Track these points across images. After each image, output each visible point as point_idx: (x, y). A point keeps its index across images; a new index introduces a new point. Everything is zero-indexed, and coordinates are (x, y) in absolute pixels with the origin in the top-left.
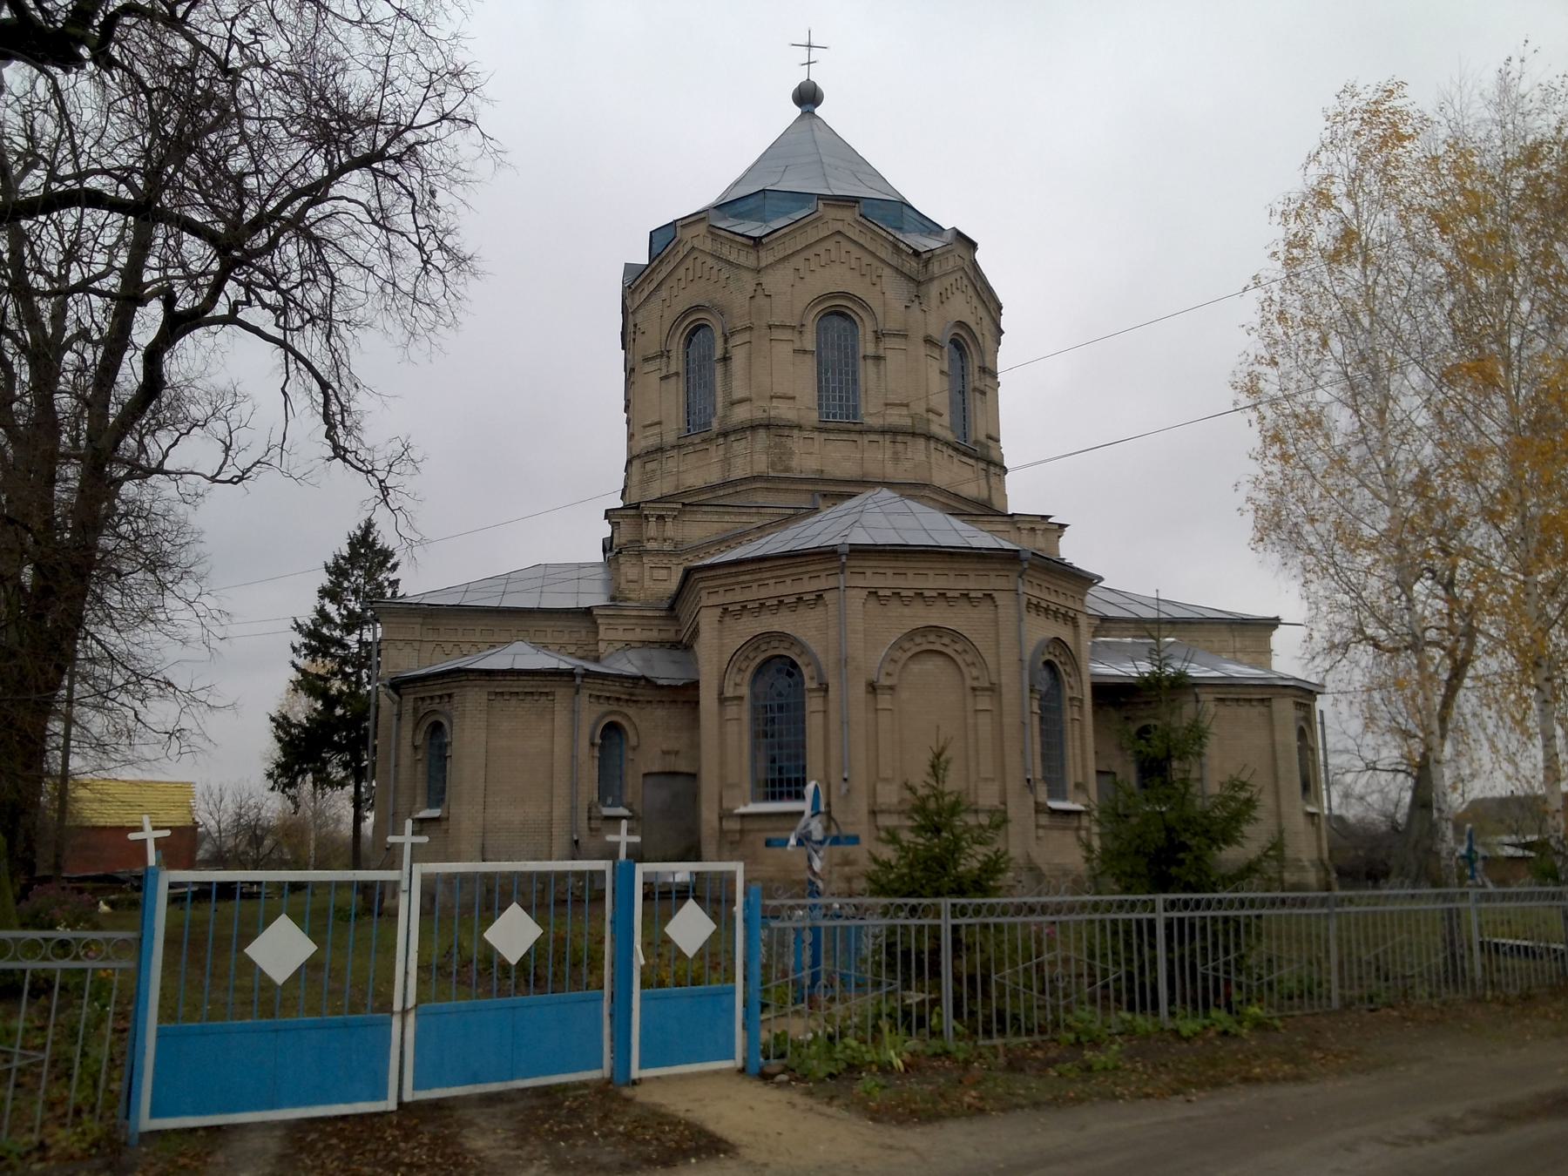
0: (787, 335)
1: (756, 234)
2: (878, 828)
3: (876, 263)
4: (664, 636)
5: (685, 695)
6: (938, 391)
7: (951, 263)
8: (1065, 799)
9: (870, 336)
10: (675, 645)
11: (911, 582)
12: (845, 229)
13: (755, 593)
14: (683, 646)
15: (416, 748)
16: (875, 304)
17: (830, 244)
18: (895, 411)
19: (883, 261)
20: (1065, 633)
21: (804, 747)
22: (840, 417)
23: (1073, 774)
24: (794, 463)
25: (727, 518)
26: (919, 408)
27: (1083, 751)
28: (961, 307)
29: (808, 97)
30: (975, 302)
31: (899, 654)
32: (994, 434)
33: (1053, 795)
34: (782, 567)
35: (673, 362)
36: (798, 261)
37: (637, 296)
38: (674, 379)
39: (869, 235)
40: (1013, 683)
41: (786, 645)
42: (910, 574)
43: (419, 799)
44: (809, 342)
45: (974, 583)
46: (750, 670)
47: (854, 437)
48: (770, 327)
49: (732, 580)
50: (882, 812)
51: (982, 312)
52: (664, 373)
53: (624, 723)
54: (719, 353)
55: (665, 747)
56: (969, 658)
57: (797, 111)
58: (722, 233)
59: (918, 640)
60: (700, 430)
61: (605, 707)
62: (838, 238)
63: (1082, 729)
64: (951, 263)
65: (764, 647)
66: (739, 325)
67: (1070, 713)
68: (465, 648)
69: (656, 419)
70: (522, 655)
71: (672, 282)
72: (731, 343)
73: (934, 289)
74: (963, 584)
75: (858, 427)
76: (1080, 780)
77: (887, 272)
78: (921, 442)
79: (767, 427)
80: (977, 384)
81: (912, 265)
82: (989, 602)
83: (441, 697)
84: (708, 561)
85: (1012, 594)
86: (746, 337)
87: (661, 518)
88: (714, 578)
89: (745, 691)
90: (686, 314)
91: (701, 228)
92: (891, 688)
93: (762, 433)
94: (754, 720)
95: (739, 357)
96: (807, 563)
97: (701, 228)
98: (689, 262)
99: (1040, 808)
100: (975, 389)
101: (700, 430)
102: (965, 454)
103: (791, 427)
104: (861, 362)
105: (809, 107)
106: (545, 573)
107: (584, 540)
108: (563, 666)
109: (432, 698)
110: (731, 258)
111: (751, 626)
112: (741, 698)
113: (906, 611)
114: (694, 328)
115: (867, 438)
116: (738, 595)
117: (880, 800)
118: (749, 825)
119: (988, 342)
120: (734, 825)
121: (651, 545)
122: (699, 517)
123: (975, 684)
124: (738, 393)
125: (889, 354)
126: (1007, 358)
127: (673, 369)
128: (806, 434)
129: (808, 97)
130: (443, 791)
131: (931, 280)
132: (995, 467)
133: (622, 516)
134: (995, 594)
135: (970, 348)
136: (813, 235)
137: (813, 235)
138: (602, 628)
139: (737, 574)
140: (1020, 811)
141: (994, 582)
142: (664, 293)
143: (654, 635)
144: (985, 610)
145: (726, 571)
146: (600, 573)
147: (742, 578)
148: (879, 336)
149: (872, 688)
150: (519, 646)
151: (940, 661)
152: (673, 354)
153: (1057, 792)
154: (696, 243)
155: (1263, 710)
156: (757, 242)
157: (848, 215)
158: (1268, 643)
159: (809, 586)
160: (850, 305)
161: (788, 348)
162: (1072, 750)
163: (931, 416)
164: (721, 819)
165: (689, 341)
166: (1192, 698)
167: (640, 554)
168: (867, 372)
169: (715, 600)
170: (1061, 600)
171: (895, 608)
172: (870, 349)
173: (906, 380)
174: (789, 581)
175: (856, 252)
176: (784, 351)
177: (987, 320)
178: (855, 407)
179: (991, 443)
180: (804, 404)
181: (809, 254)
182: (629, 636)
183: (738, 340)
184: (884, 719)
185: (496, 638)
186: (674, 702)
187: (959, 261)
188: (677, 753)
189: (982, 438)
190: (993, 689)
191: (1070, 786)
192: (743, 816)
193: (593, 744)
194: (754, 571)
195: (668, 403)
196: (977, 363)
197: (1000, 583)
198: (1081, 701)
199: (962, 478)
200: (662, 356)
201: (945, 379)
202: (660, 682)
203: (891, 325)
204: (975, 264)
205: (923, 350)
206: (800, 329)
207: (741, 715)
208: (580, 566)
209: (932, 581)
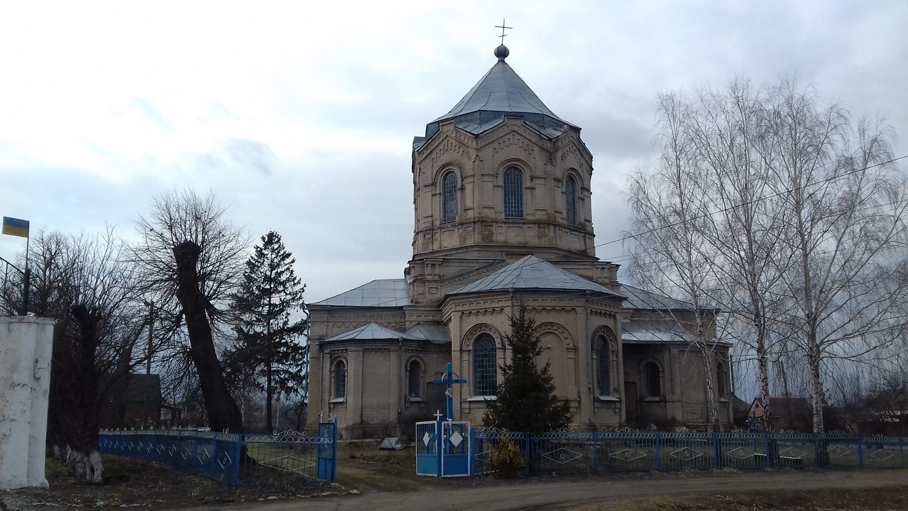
0: (490, 179)
3: (531, 144)
4: (435, 318)
5: (446, 348)
6: (561, 203)
7: (567, 140)
8: (609, 395)
9: (528, 178)
10: (438, 323)
14: (442, 324)
15: (331, 372)
17: (510, 136)
18: (539, 213)
20: (609, 322)
23: (613, 384)
24: (494, 238)
26: (550, 211)
27: (618, 375)
28: (572, 161)
29: (502, 53)
30: (579, 156)
32: (588, 218)
33: (602, 394)
34: (487, 296)
35: (438, 188)
36: (496, 145)
40: (584, 347)
42: (540, 300)
44: (500, 181)
45: (566, 303)
51: (583, 161)
54: (459, 186)
55: (437, 371)
56: (565, 335)
57: (497, 59)
60: (448, 220)
61: (409, 355)
63: (617, 365)
64: (567, 140)
66: (468, 174)
67: (612, 358)
70: (374, 331)
71: (437, 151)
72: (466, 181)
73: (559, 155)
74: (563, 304)
76: (616, 386)
77: (536, 149)
79: (482, 222)
80: (580, 195)
81: (548, 145)
84: (455, 292)
85: (583, 309)
86: (471, 179)
87: (433, 265)
89: (471, 348)
90: (444, 166)
91: (451, 127)
93: (478, 225)
94: (475, 361)
98: (445, 142)
99: (596, 400)
100: (579, 198)
101: (448, 220)
103: (493, 222)
104: (524, 191)
106: (377, 285)
107: (394, 267)
108: (395, 337)
112: (469, 351)
114: (446, 172)
115: (526, 226)
116: (467, 307)
118: (473, 406)
119: (585, 175)
120: (466, 406)
121: (429, 278)
124: (469, 204)
125: (537, 187)
126: (596, 183)
127: (438, 192)
129: (502, 53)
132: (589, 234)
135: (576, 183)
138: (407, 315)
140: (586, 400)
141: (575, 303)
142: (434, 155)
143: (430, 318)
144: (571, 316)
146: (402, 286)
148: (532, 178)
150: (373, 326)
151: (553, 337)
152: (438, 184)
153: (605, 391)
154: (449, 133)
156: (477, 137)
157: (519, 123)
161: (491, 185)
162: (613, 373)
163: (557, 214)
167: (424, 282)
168: (527, 196)
170: (608, 308)
173: (541, 199)
177: (585, 165)
178: (522, 211)
179: (587, 223)
181: (501, 141)
182: (420, 319)
186: (440, 351)
187: (571, 139)
189: (583, 221)
190: (575, 349)
191: (612, 389)
192: (470, 402)
195: (435, 208)
196: (580, 185)
197: (579, 304)
198: (617, 352)
199: (573, 242)
201: (564, 196)
203: (537, 174)
204: (579, 139)
205: (553, 183)
206: (496, 176)
208: (394, 281)
209: (549, 303)
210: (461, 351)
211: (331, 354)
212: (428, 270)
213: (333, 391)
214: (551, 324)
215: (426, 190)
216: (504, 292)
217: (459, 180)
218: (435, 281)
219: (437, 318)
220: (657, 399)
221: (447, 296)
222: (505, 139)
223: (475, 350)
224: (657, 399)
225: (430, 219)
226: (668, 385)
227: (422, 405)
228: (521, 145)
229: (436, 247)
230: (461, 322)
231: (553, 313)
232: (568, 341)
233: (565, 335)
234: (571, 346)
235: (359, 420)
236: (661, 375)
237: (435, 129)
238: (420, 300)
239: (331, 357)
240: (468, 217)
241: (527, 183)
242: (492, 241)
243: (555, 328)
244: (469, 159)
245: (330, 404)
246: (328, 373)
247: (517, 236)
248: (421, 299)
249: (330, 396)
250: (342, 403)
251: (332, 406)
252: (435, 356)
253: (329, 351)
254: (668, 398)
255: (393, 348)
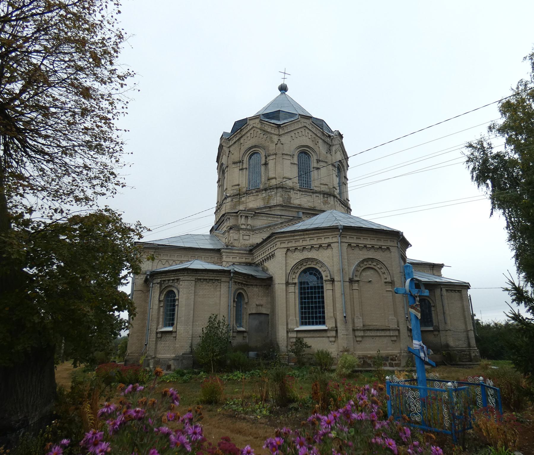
0: (289, 157)
1: (279, 123)
2: (356, 336)
3: (317, 138)
4: (247, 261)
9: (315, 161)
11: (362, 242)
12: (307, 126)
13: (300, 243)
15: (160, 301)
16: (317, 150)
17: (302, 130)
18: (322, 186)
19: (319, 137)
21: (323, 302)
22: (306, 188)
25: (269, 219)
29: (283, 89)
31: (359, 268)
34: (314, 234)
36: (292, 134)
37: (231, 142)
38: (245, 170)
39: (315, 129)
41: (315, 263)
43: (161, 323)
46: (299, 273)
47: (311, 194)
48: (283, 154)
49: (292, 238)
50: (357, 330)
52: (241, 168)
53: (243, 293)
54: (263, 162)
57: (280, 93)
58: (265, 122)
59: (365, 263)
61: (237, 287)
62: (305, 128)
65: (305, 264)
66: (272, 153)
68: (171, 262)
69: (237, 183)
70: (197, 264)
72: (268, 158)
74: (380, 243)
75: (312, 191)
77: (320, 141)
78: (332, 198)
82: (388, 251)
83: (173, 280)
84: (282, 230)
86: (274, 157)
87: (247, 217)
88: (284, 237)
89: (296, 281)
90: (250, 148)
91: (257, 121)
92: (358, 281)
95: (271, 163)
96: (324, 232)
97: (257, 121)
98: (252, 131)
102: (342, 204)
103: (291, 189)
105: (283, 91)
109: (169, 280)
110: (269, 130)
111: (298, 256)
112: (295, 284)
113: (360, 252)
115: (315, 195)
116: (293, 244)
117: (356, 325)
122: (260, 218)
123: (386, 281)
124: (271, 175)
128: (295, 192)
129: (283, 89)
130: (173, 320)
131: (333, 145)
133: (231, 216)
134: (390, 248)
136: (297, 126)
137: (297, 126)
138: (224, 257)
139: (294, 236)
143: (243, 260)
145: (289, 234)
147: (295, 237)
148: (318, 161)
149: (351, 281)
150: (197, 262)
151: (372, 271)
152: (245, 162)
155: (459, 294)
156: (279, 126)
158: (440, 272)
159: (324, 241)
160: (309, 150)
161: (289, 162)
164: (287, 332)
165: (250, 157)
166: (440, 289)
168: (314, 174)
169: (283, 245)
171: (357, 251)
172: (315, 165)
173: (323, 177)
174: (316, 239)
175: (310, 133)
176: (287, 163)
180: (294, 182)
181: (296, 132)
182: (234, 260)
183: (271, 158)
184: (356, 293)
185: (183, 259)
186: (261, 286)
188: (262, 306)
193: (234, 301)
194: (301, 235)
197: (392, 244)
200: (240, 162)
202: (258, 277)
204: (342, 143)
207: (294, 292)
209: (369, 242)
210: (287, 284)
211: (160, 284)
212: (243, 220)
213: (161, 320)
214: (372, 259)
215: (234, 166)
216: (333, 229)
217: (264, 158)
218: (249, 230)
219: (249, 260)
220: (431, 329)
221: (273, 234)
222: (299, 131)
223: (301, 283)
224: (431, 329)
225: (237, 187)
226: (441, 317)
227: (245, 335)
228: (310, 137)
229: (241, 207)
230: (286, 257)
231: (373, 250)
232: (385, 276)
233: (383, 270)
234: (389, 280)
235: (189, 350)
236: (433, 309)
237: (240, 126)
238: (235, 245)
239: (161, 286)
240: (271, 184)
241: (314, 164)
242: (291, 203)
243: (374, 264)
244: (272, 142)
245: (157, 333)
246: (157, 302)
247: (308, 201)
248: (236, 244)
249: (158, 324)
250: (171, 332)
251: (159, 335)
252: (256, 289)
253: (159, 281)
254: (441, 328)
255: (223, 279)
